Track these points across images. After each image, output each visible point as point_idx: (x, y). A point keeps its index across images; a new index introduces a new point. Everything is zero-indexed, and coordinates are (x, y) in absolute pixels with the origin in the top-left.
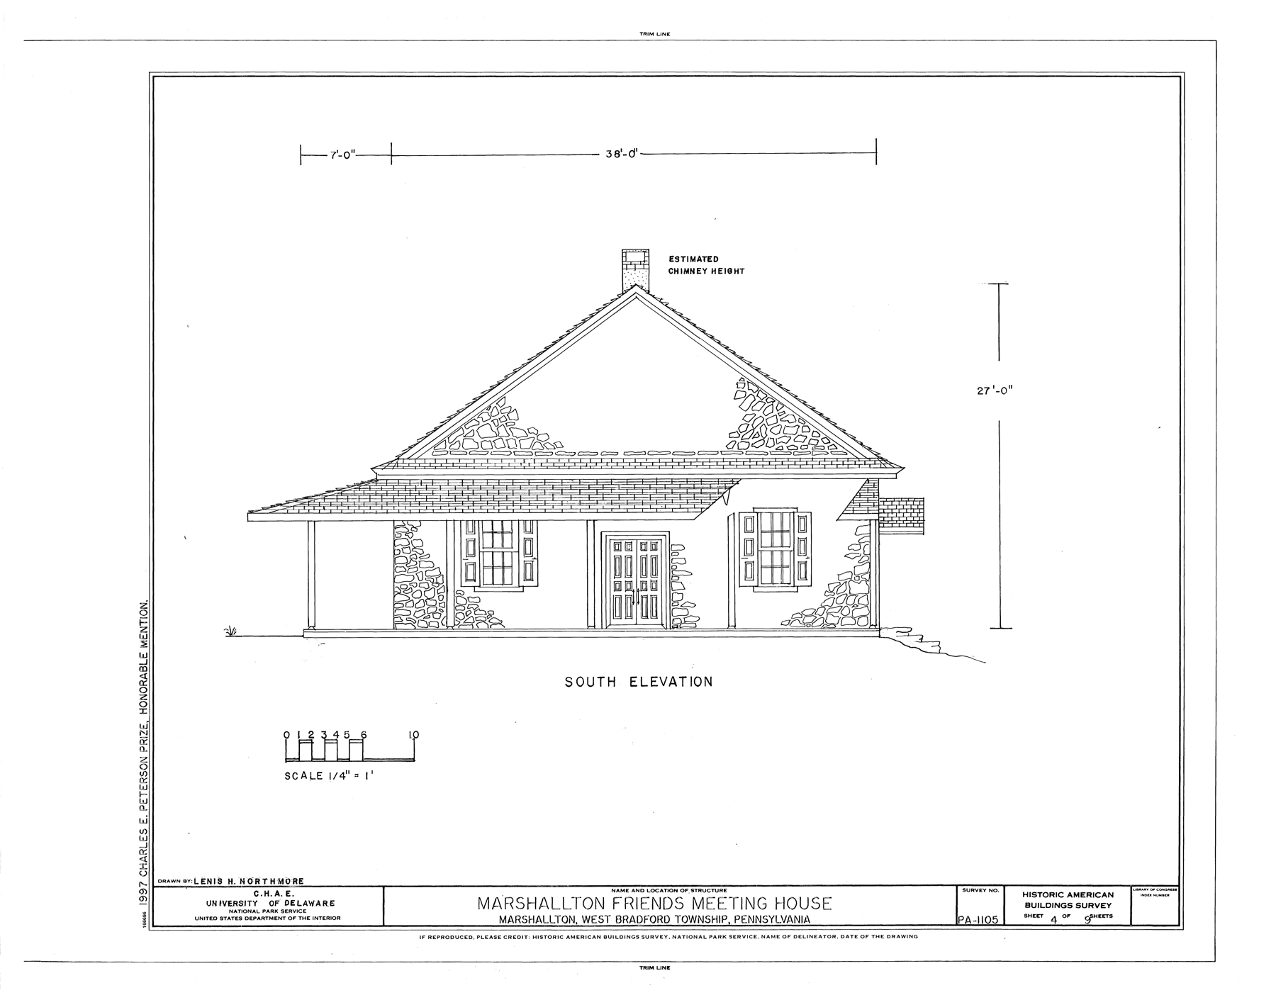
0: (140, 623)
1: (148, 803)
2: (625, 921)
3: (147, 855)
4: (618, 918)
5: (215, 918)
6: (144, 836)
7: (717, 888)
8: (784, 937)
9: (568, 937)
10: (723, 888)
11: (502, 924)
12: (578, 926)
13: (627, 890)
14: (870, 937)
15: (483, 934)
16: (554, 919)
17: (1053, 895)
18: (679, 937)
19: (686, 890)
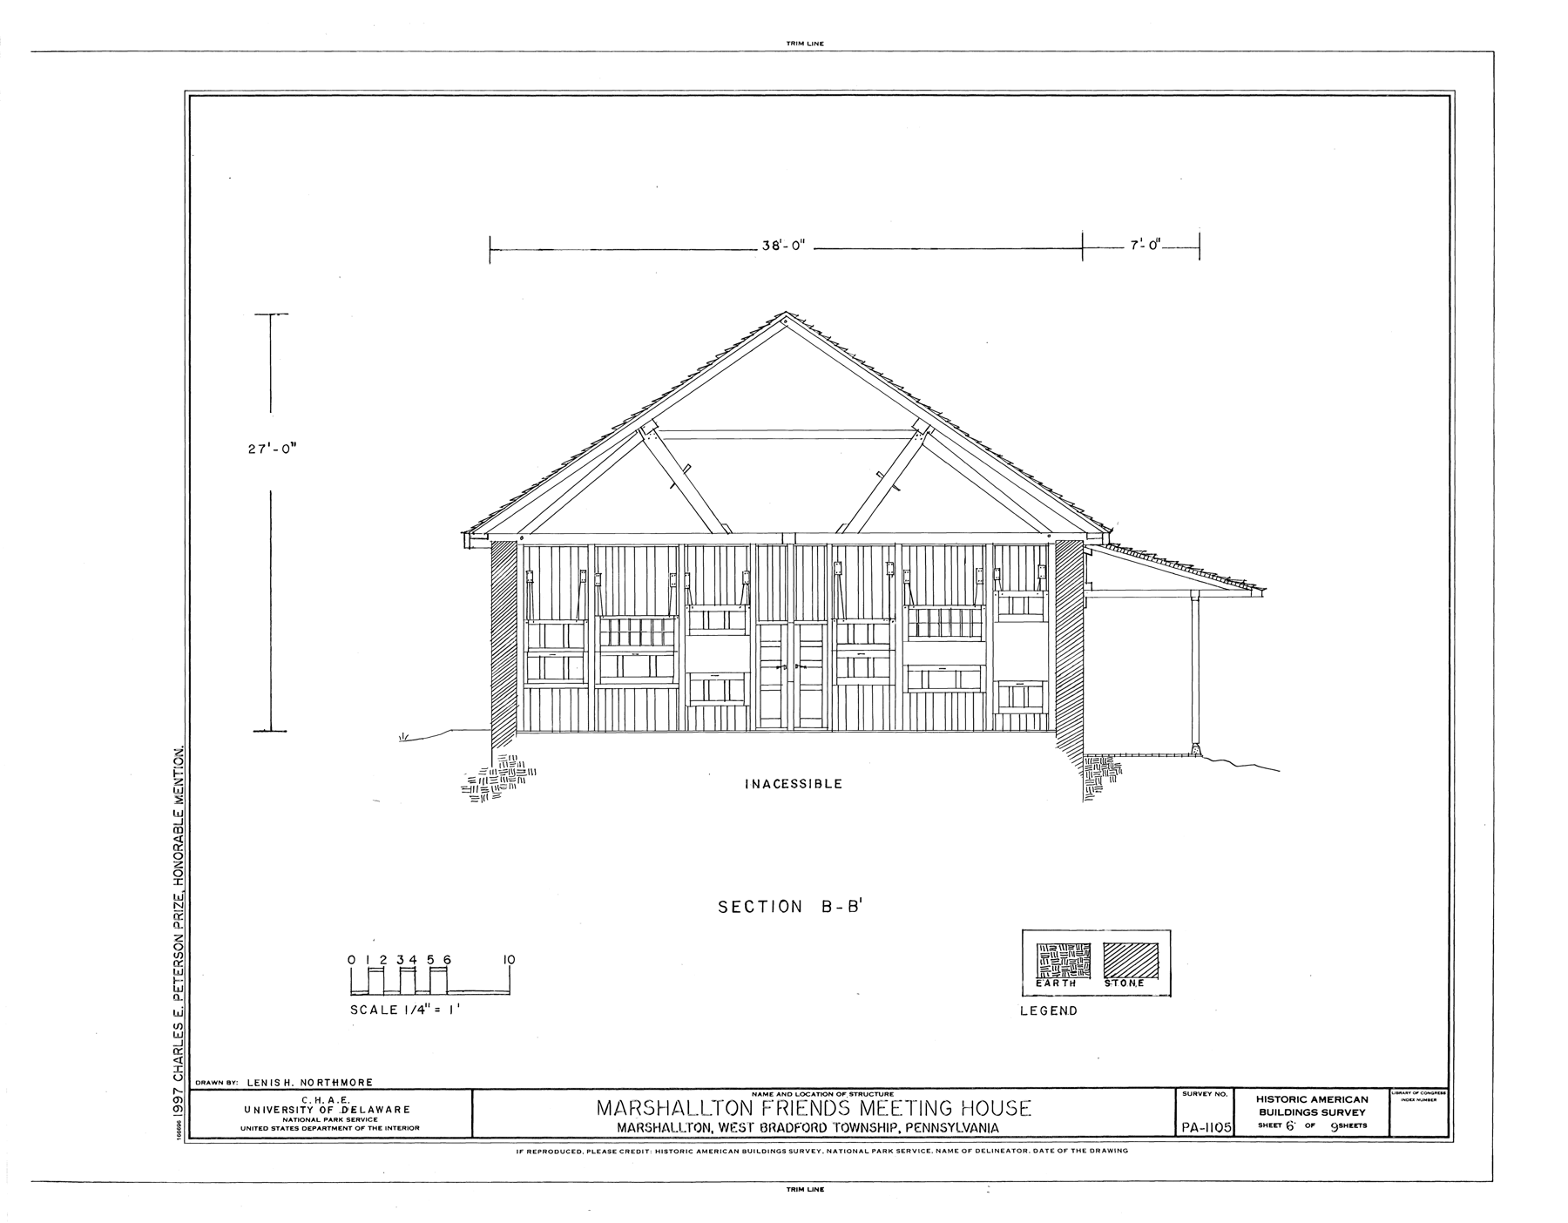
0: (175, 774)
2: (772, 1130)
4: (764, 1125)
5: (266, 1129)
6: (179, 1031)
7: (881, 1091)
8: (964, 1151)
9: (699, 1151)
10: (889, 1091)
14: (1069, 1151)
15: (594, 1147)
17: (1294, 1100)
18: (835, 1151)
19: (844, 1094)
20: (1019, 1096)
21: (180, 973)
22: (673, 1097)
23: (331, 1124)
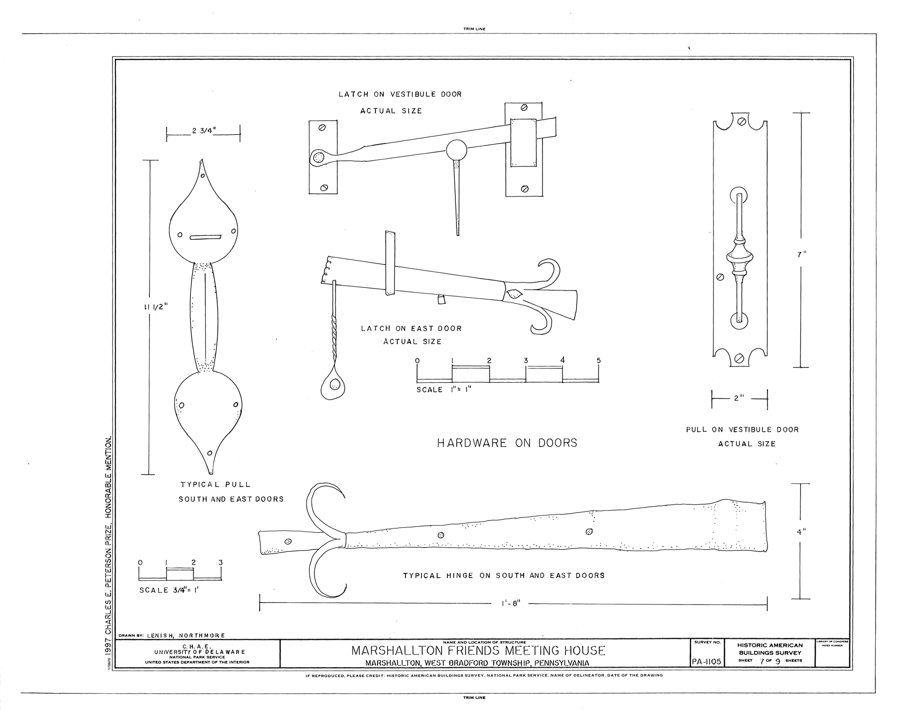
2: (456, 664)
3: (111, 619)
4: (451, 662)
5: (160, 662)
6: (108, 605)
7: (519, 641)
8: (567, 675)
9: (412, 676)
10: (523, 641)
11: (367, 666)
13: (454, 642)
14: (629, 675)
15: (351, 673)
16: (405, 663)
17: (759, 646)
18: (492, 675)
19: (497, 642)
20: (598, 643)
22: (396, 644)
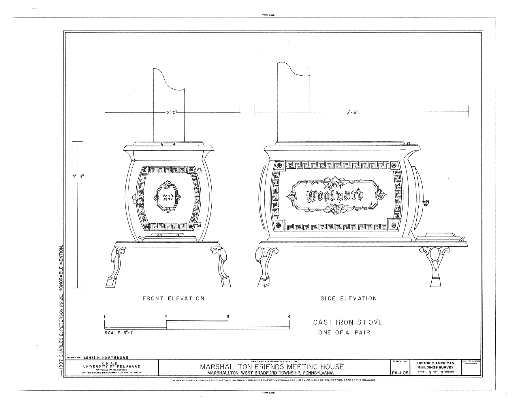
0: (60, 254)
1: (63, 327)
2: (259, 374)
3: (63, 349)
4: (256, 372)
5: (90, 373)
6: (61, 341)
7: (293, 360)
9: (233, 380)
10: (296, 360)
12: (240, 376)
14: (356, 380)
15: (199, 379)
17: (430, 363)
19: (281, 361)
21: (62, 321)
23: (112, 371)
